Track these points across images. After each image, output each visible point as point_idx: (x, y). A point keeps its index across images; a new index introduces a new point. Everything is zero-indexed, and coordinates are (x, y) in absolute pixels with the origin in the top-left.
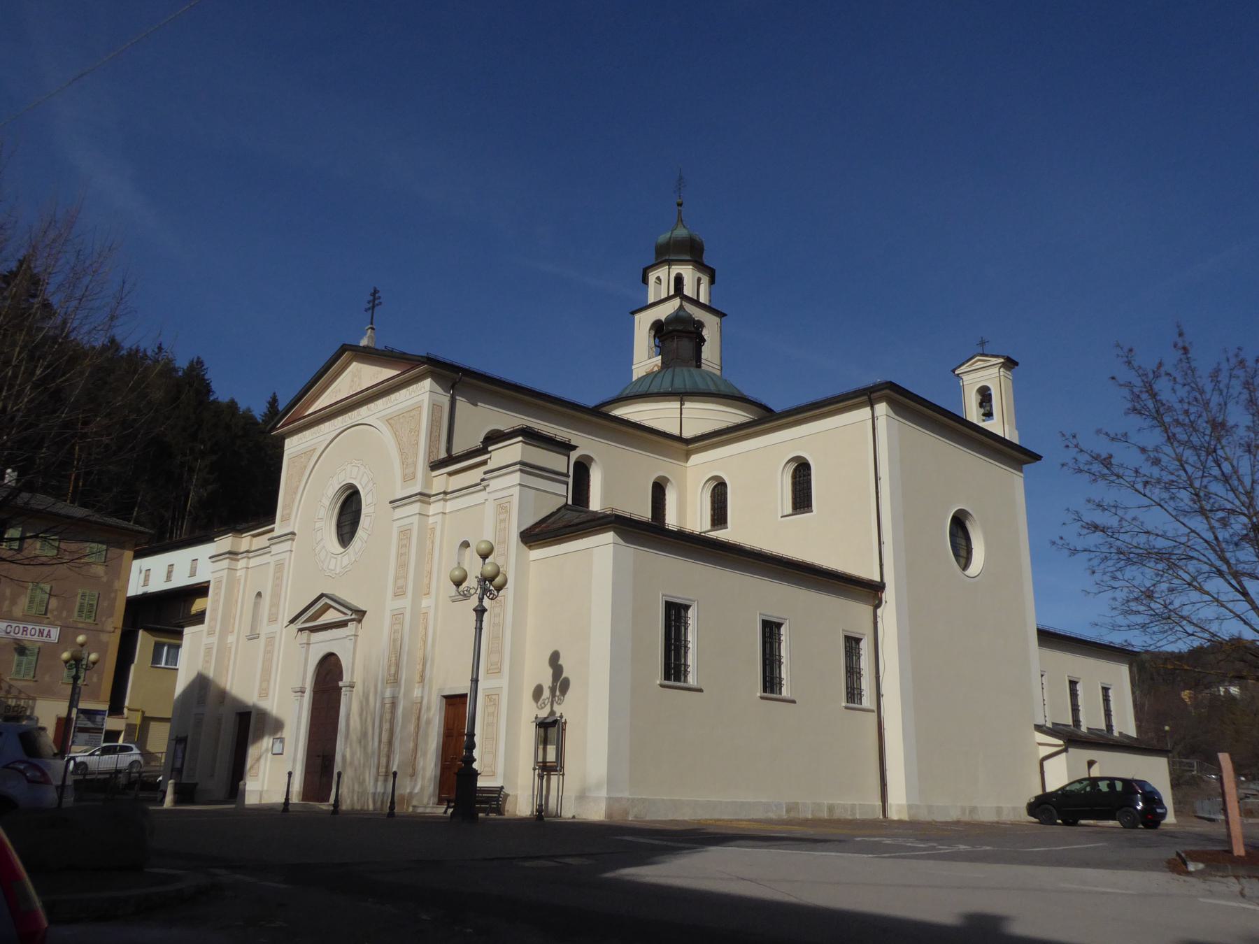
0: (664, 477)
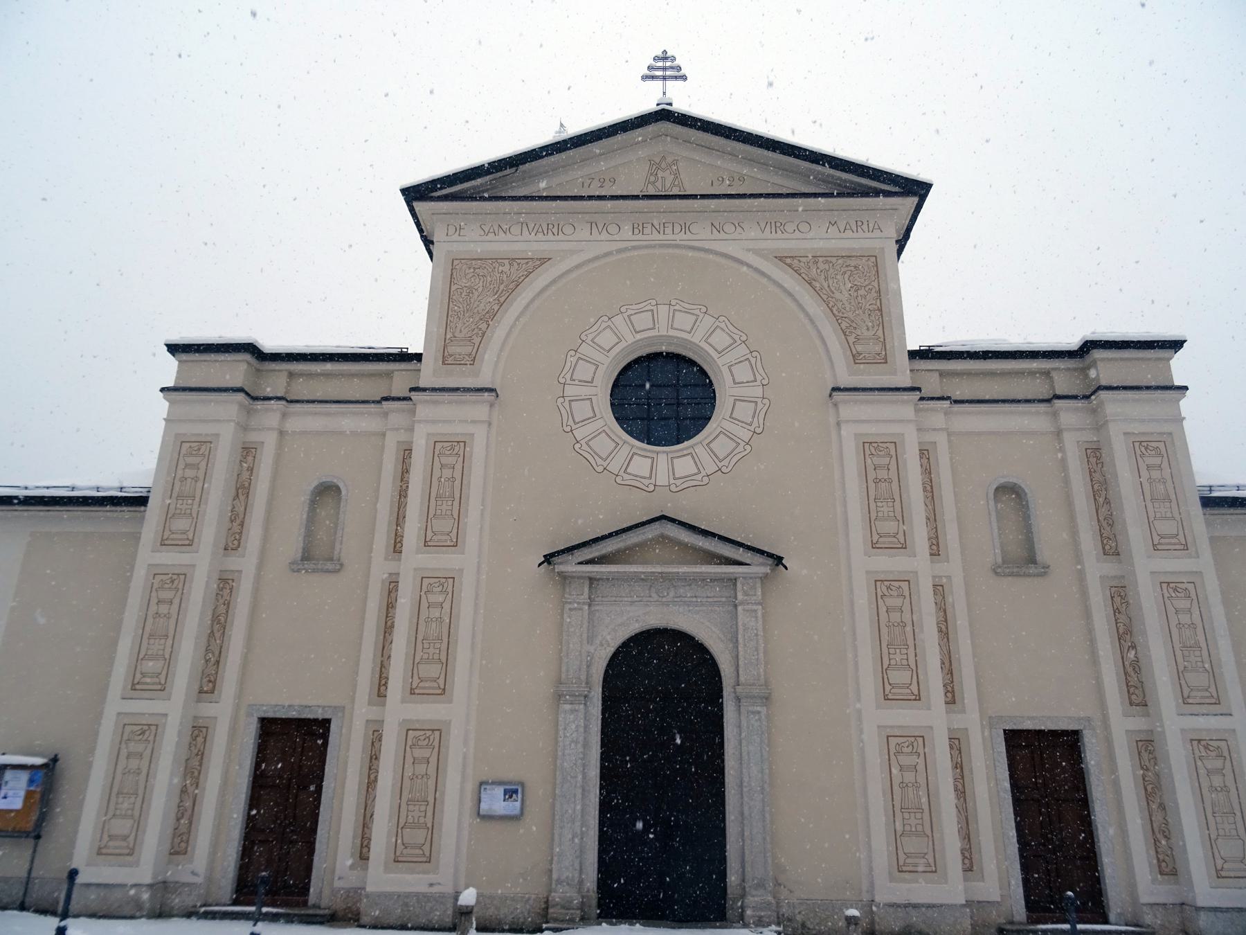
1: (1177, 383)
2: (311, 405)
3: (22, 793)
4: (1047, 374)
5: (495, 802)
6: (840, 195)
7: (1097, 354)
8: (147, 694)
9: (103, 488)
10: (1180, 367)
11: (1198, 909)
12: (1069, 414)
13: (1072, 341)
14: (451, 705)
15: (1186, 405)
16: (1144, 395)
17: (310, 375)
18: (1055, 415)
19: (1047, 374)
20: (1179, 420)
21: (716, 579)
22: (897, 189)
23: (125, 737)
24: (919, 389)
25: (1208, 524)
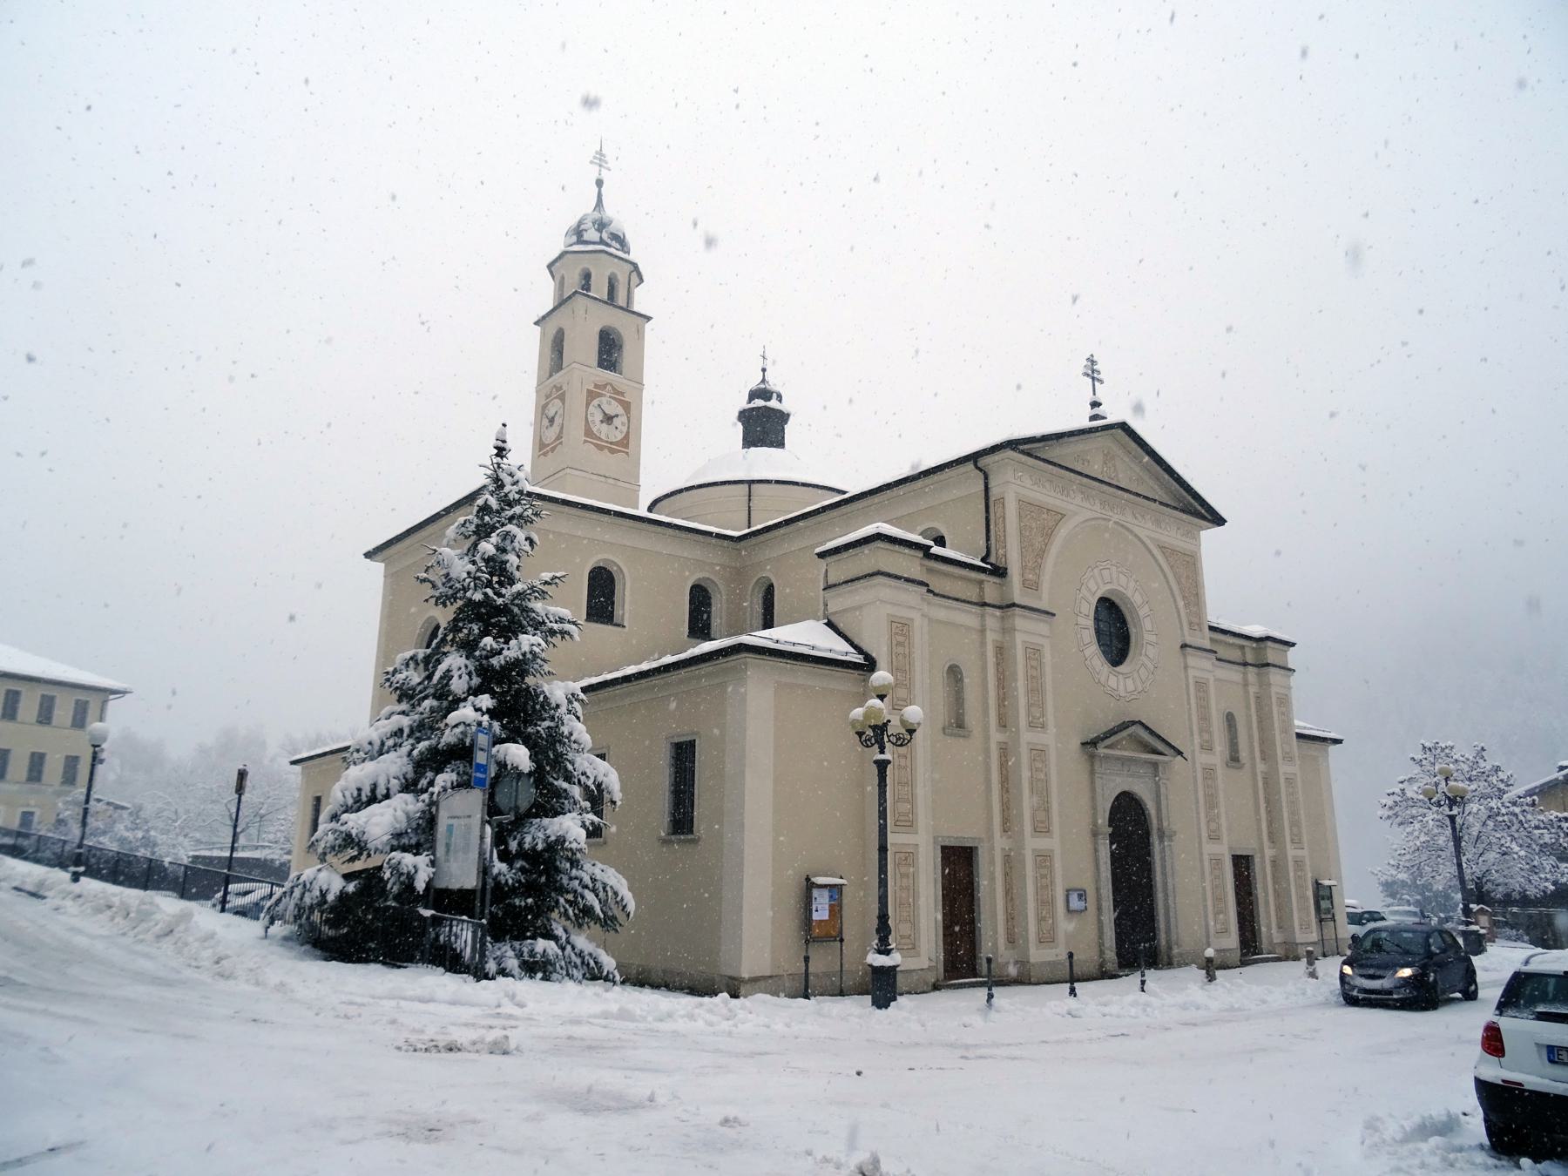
0: (713, 582)
1: (1290, 666)
2: (944, 600)
3: (827, 907)
4: (1242, 647)
5: (1075, 903)
6: (1183, 511)
7: (1269, 644)
8: (904, 829)
9: (834, 651)
10: (1293, 657)
11: (1297, 944)
12: (992, 618)
13: (1256, 630)
14: (33, 750)
15: (1295, 680)
16: (1035, 615)
17: (946, 574)
18: (983, 616)
19: (1242, 647)
20: (1289, 688)
21: (1146, 762)
22: (1210, 518)
23: (897, 862)
24: (1215, 652)
25: (1299, 747)
